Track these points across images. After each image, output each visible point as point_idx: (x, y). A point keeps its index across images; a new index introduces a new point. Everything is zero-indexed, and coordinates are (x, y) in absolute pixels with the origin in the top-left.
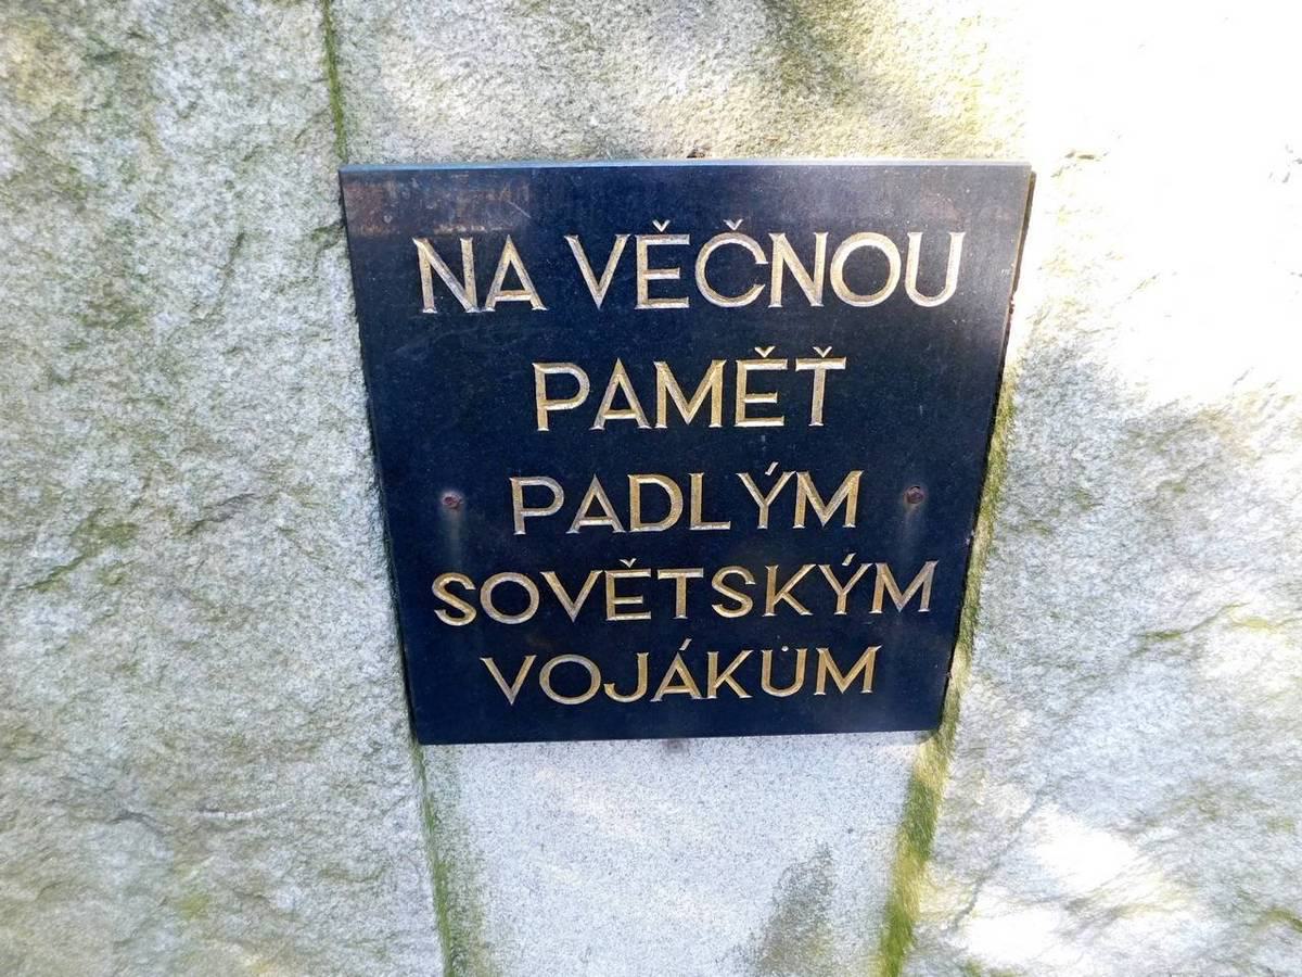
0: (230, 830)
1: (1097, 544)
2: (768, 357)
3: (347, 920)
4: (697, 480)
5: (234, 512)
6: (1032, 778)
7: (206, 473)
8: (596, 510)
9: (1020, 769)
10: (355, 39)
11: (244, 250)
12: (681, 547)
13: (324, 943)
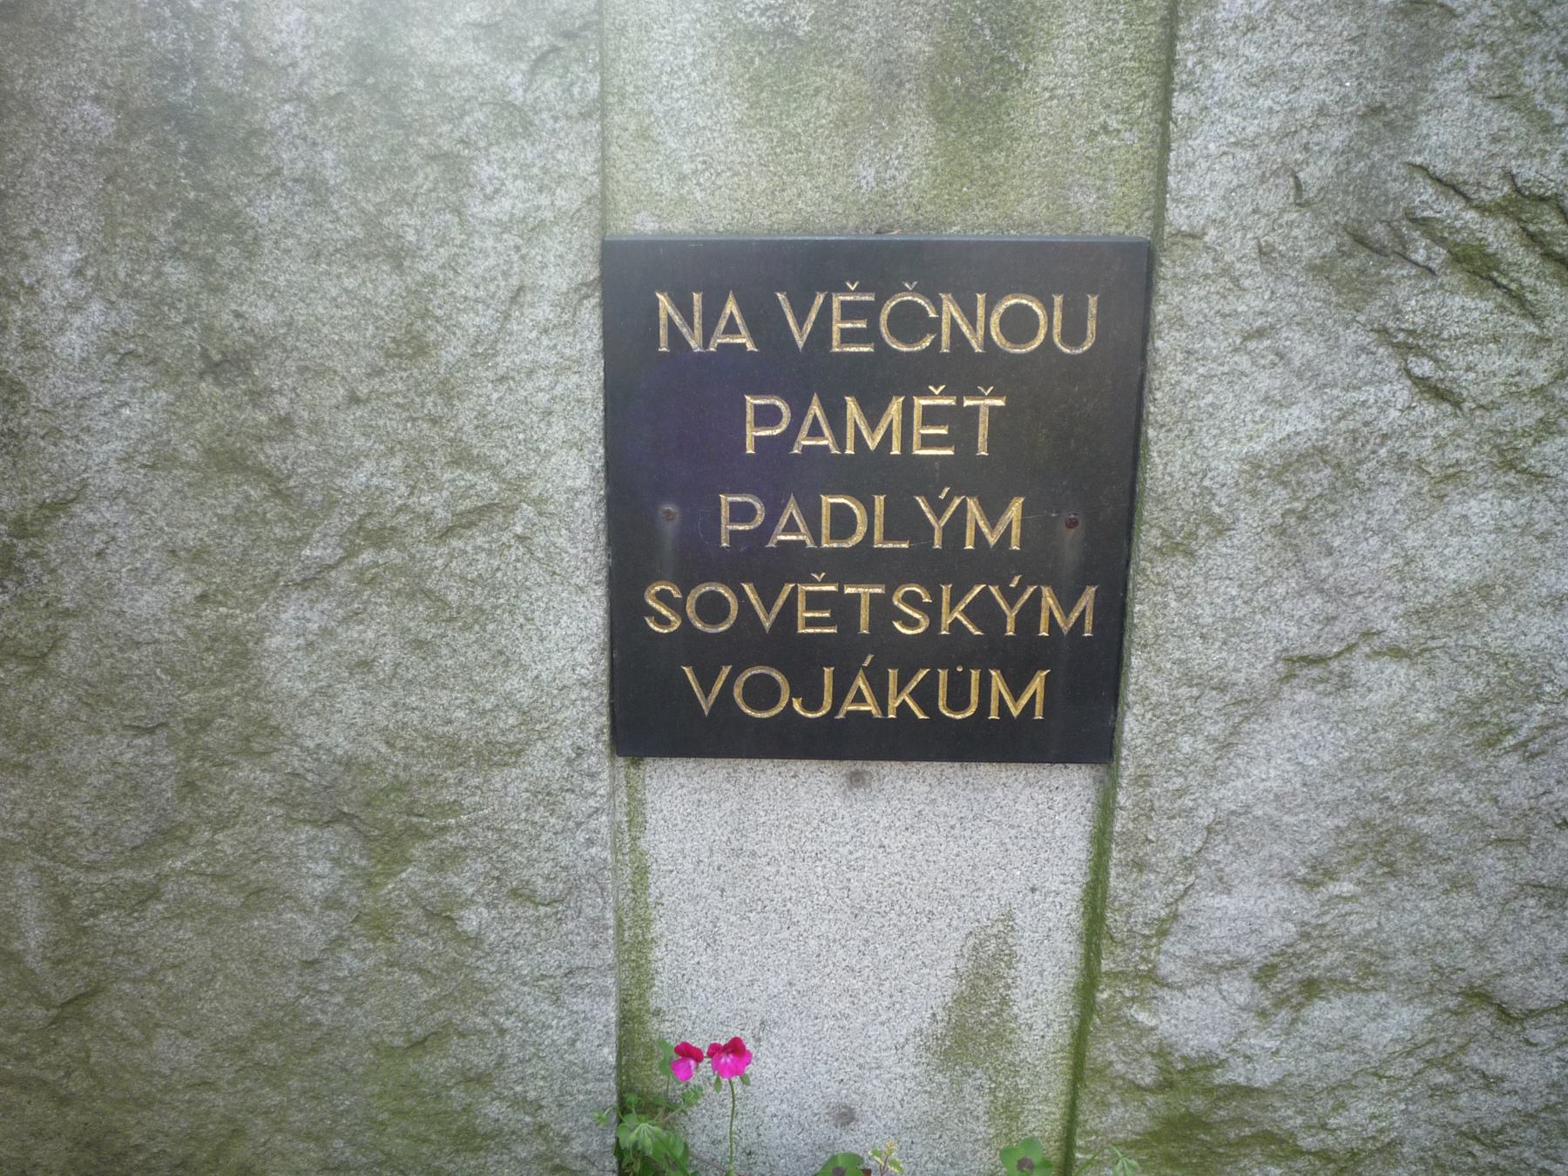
0: (433, 837)
1: (1234, 566)
2: (941, 394)
3: (528, 951)
4: (879, 501)
5: (480, 520)
6: (1201, 813)
7: (463, 483)
8: (791, 527)
9: (1188, 802)
10: (621, 143)
11: (521, 299)
12: (863, 563)
13: (502, 978)
